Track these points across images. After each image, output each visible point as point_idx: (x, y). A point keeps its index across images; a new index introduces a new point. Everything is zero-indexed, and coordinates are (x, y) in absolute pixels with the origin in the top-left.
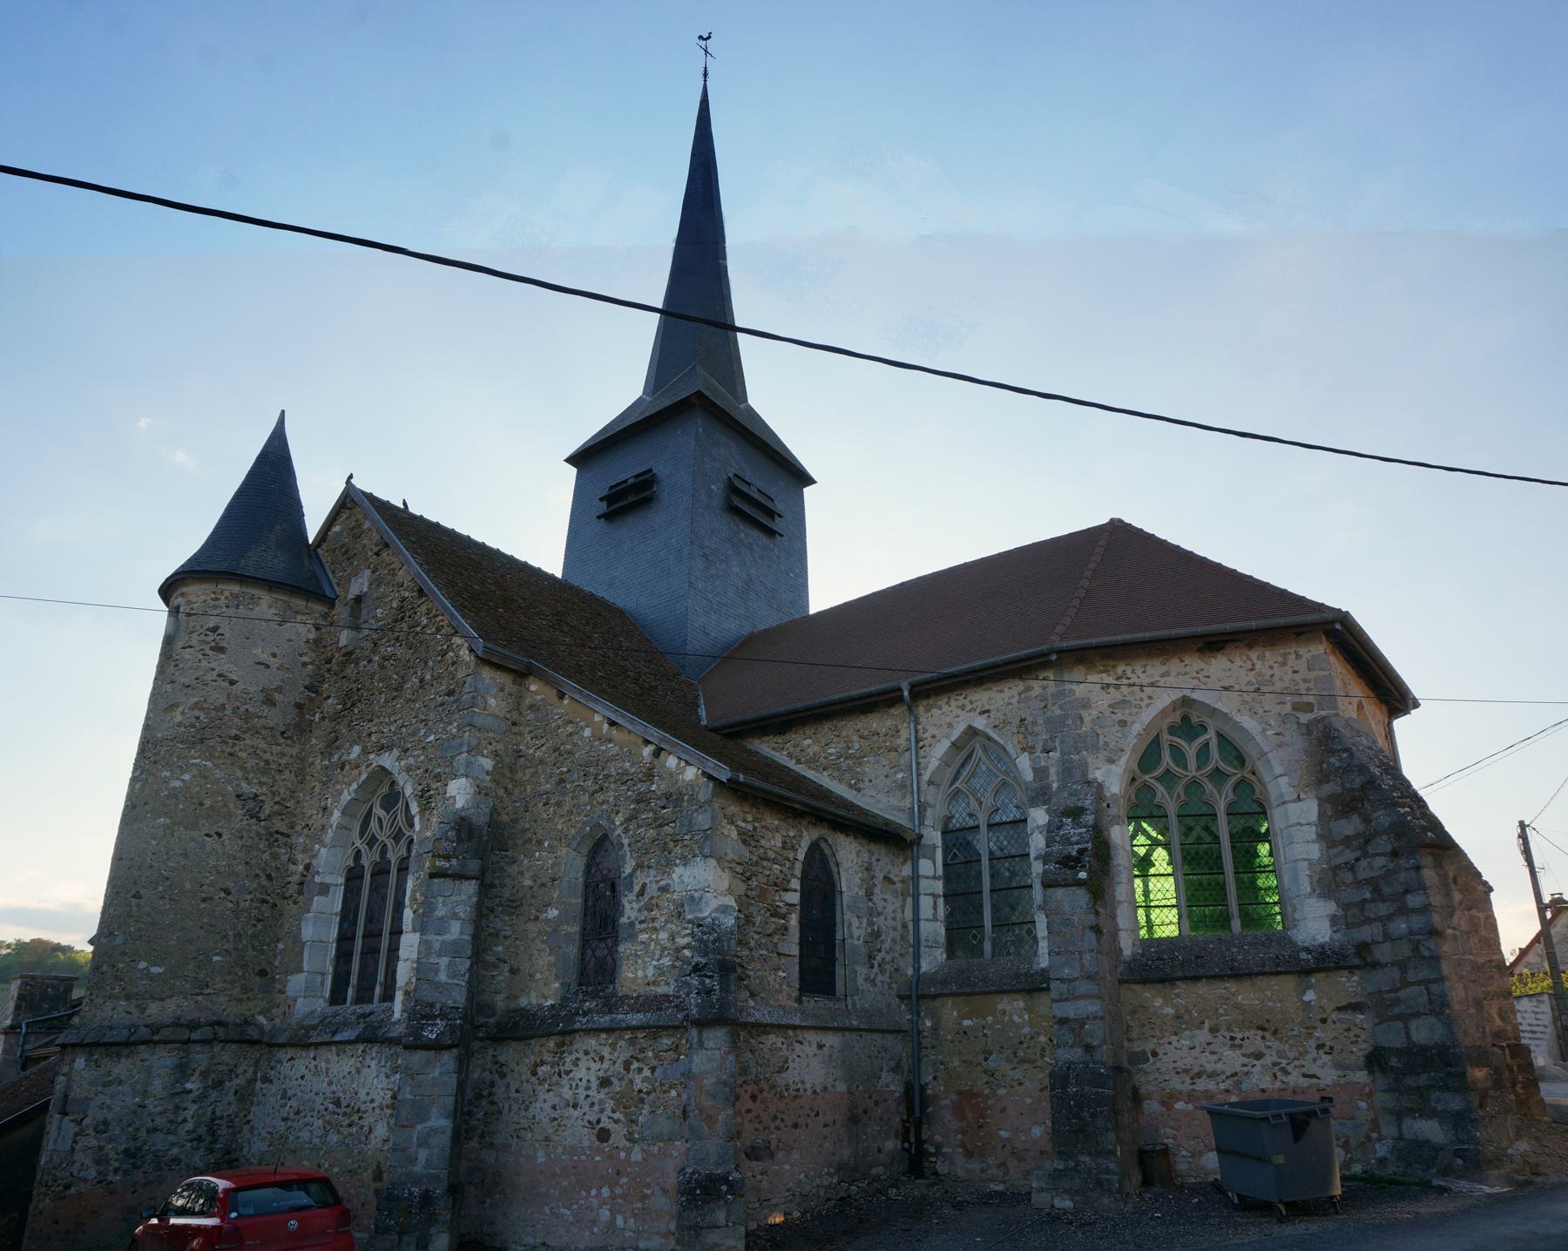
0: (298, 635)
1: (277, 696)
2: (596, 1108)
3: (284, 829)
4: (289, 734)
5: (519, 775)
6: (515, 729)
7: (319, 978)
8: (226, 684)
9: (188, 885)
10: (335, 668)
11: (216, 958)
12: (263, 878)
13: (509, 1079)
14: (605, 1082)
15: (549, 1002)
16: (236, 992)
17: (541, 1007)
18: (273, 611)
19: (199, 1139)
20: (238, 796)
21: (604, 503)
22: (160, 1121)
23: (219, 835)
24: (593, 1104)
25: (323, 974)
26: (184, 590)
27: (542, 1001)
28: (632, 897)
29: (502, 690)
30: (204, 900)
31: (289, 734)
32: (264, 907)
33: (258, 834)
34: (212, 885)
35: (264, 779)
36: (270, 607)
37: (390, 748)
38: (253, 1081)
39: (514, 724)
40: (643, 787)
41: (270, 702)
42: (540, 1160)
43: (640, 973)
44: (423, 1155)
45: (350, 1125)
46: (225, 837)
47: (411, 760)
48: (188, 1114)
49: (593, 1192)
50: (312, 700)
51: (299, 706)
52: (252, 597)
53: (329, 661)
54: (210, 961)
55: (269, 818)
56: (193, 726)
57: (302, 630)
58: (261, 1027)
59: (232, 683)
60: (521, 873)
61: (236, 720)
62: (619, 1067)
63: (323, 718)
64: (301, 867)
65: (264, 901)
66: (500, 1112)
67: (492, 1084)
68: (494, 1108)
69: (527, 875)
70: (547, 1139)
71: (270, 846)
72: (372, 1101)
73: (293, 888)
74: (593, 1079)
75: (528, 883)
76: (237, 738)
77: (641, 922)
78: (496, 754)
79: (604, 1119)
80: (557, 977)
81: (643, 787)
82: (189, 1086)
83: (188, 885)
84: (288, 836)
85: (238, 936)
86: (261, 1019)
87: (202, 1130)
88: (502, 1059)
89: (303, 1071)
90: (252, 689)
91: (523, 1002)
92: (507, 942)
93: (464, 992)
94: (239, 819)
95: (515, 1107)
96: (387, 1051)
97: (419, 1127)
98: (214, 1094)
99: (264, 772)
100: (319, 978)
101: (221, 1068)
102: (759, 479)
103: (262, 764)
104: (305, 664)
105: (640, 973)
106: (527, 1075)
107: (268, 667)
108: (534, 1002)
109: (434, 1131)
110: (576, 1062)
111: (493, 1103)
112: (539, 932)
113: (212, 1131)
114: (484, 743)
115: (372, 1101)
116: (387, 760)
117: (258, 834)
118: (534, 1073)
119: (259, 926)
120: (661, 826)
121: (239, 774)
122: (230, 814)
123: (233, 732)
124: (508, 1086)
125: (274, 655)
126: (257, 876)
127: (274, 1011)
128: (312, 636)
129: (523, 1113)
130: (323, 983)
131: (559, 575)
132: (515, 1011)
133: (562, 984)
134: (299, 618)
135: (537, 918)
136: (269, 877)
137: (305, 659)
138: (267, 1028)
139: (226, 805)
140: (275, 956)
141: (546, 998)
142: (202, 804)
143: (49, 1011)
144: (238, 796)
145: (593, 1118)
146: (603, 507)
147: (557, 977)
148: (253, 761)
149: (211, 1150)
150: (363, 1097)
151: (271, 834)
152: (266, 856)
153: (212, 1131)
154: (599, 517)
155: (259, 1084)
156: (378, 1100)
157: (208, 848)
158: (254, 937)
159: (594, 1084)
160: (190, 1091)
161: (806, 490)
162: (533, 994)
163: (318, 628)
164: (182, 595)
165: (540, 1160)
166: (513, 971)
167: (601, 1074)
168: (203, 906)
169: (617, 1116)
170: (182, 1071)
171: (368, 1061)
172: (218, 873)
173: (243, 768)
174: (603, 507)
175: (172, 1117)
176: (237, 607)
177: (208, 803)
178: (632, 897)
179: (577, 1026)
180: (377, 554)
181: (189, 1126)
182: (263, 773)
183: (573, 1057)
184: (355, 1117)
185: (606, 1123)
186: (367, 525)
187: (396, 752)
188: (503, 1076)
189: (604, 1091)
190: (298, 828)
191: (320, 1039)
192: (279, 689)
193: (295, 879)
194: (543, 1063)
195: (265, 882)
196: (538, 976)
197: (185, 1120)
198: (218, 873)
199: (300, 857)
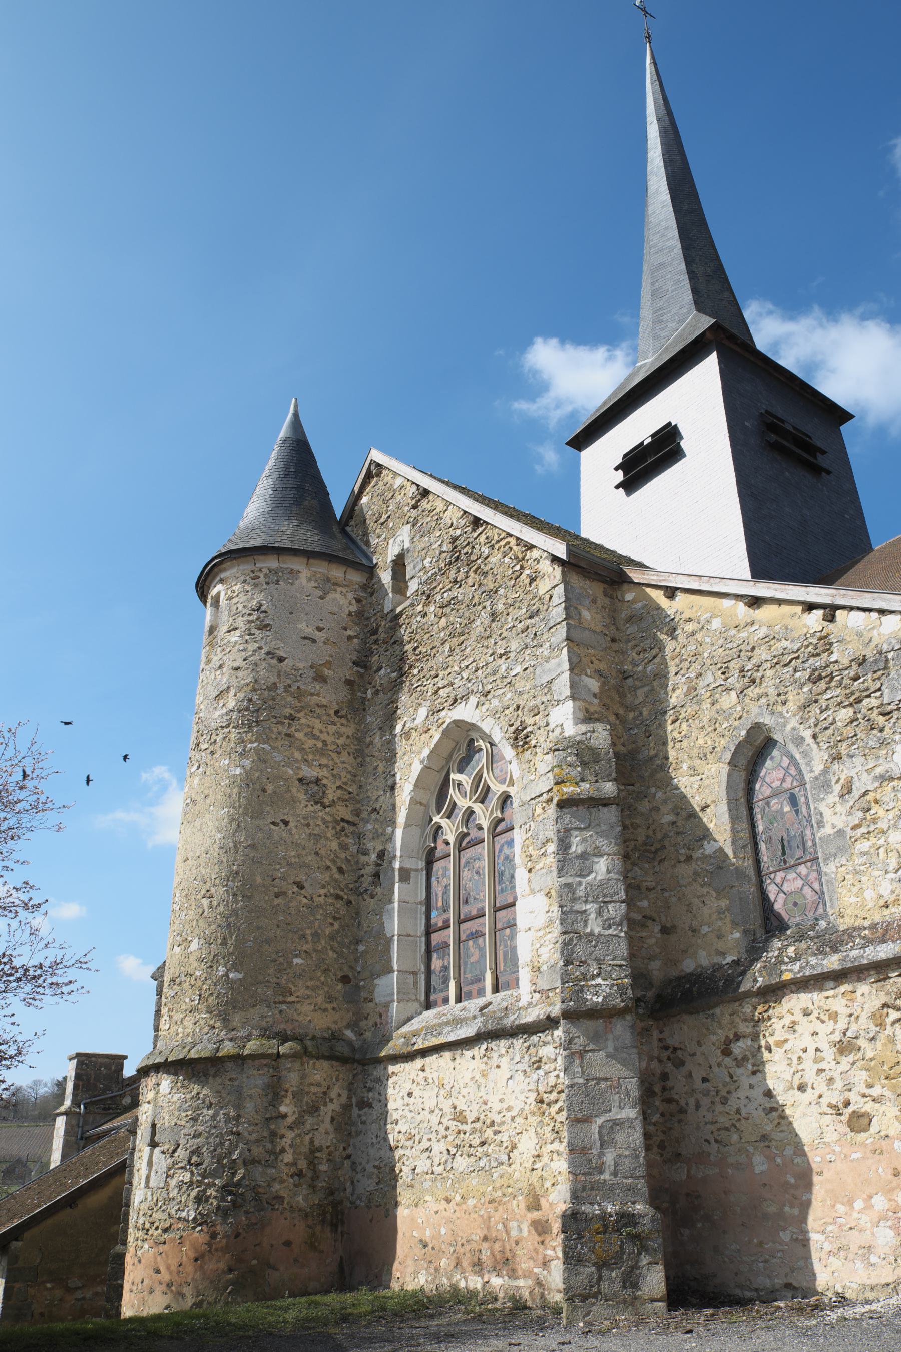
0: (341, 607)
1: (327, 672)
2: (839, 1084)
3: (349, 817)
4: (343, 712)
5: (629, 698)
6: (615, 646)
7: (411, 980)
8: (274, 662)
9: (259, 879)
10: (383, 636)
11: (297, 961)
12: (335, 870)
13: (689, 1065)
14: (845, 1047)
15: (729, 959)
16: (320, 1000)
17: (718, 968)
18: (313, 584)
19: (300, 1174)
20: (300, 780)
21: (620, 472)
22: (257, 1151)
23: (286, 823)
24: (831, 1080)
25: (415, 974)
26: (223, 575)
27: (717, 960)
28: (833, 798)
29: (594, 602)
30: (277, 896)
31: (343, 712)
32: (339, 904)
33: (325, 822)
34: (283, 878)
35: (324, 761)
36: (309, 580)
37: (465, 697)
38: (347, 1107)
39: (613, 640)
40: (818, 662)
41: (320, 678)
42: (758, 1169)
43: (869, 894)
44: (609, 1158)
45: (483, 1144)
46: (291, 825)
47: (495, 702)
48: (286, 1142)
49: (859, 1204)
50: (361, 676)
51: (349, 683)
52: (292, 571)
53: (375, 632)
54: (290, 964)
55: (333, 804)
56: (247, 709)
57: (343, 602)
58: (350, 1043)
59: (281, 660)
60: (657, 809)
61: (289, 699)
62: (865, 1023)
63: (377, 693)
64: (374, 857)
65: (338, 897)
66: (682, 1111)
67: (665, 1076)
68: (673, 1107)
69: (664, 809)
70: (764, 1137)
71: (337, 835)
72: (509, 1109)
73: (367, 881)
74: (824, 1046)
75: (668, 818)
76: (292, 718)
77: (855, 828)
78: (599, 674)
79: (853, 1097)
80: (735, 924)
81: (818, 662)
82: (283, 1109)
83: (259, 879)
84: (354, 824)
85: (316, 935)
86: (349, 1033)
87: (303, 1164)
88: (672, 1041)
89: (408, 1086)
90: (301, 665)
91: (688, 966)
92: (652, 895)
93: (624, 945)
94: (304, 807)
95: (705, 1102)
96: (518, 1042)
97: (599, 1121)
98: (310, 1121)
99: (322, 752)
100: (411, 980)
101: (314, 1089)
102: (794, 418)
103: (320, 744)
104: (350, 638)
105: (869, 894)
106: (716, 1056)
107: (314, 641)
108: (705, 962)
109: (616, 1124)
110: (792, 1027)
111: (669, 1101)
112: (696, 874)
113: (312, 1164)
114: (585, 661)
115: (509, 1109)
116: (465, 712)
117: (325, 822)
118: (727, 1052)
119: (337, 925)
120: (859, 701)
121: (298, 755)
122: (294, 800)
123: (288, 711)
124: (690, 1075)
125: (319, 629)
126: (328, 868)
127: (363, 1023)
128: (354, 608)
129: (719, 1108)
130: (416, 983)
131: (715, 353)
132: (679, 979)
133: (745, 932)
134: (339, 589)
135: (689, 858)
136: (341, 870)
137: (349, 633)
138: (357, 1044)
139: (288, 791)
140: (356, 960)
141: (723, 954)
142: (264, 790)
143: (104, 1091)
144: (300, 780)
145: (835, 1098)
146: (620, 476)
147: (735, 924)
148: (311, 742)
149: (313, 1187)
150: (497, 1106)
151: (336, 821)
152: (334, 845)
153: (312, 1164)
154: (617, 487)
155: (355, 1111)
156: (517, 1105)
157: (276, 838)
158: (332, 938)
159: (829, 1053)
160: (284, 1116)
161: (842, 428)
162: (702, 954)
163: (358, 601)
164: (222, 581)
165: (758, 1169)
166: (665, 930)
167: (837, 1037)
168: (276, 901)
169: (876, 1091)
170: (274, 1092)
171: (495, 1060)
172: (288, 864)
173: (301, 749)
174: (620, 476)
175: (269, 1146)
176: (277, 583)
177: (270, 788)
178: (833, 798)
179: (787, 976)
180: (415, 507)
181: (288, 1157)
182: (322, 754)
183: (787, 1020)
184: (489, 1133)
185: (858, 1104)
186: (399, 481)
187: (473, 700)
188: (681, 1063)
189: (846, 1061)
190: (364, 815)
191: (428, 1044)
192: (328, 665)
193: (369, 870)
194: (737, 1037)
195: (337, 876)
196: (705, 929)
197: (283, 1150)
198: (288, 864)
199: (370, 845)
